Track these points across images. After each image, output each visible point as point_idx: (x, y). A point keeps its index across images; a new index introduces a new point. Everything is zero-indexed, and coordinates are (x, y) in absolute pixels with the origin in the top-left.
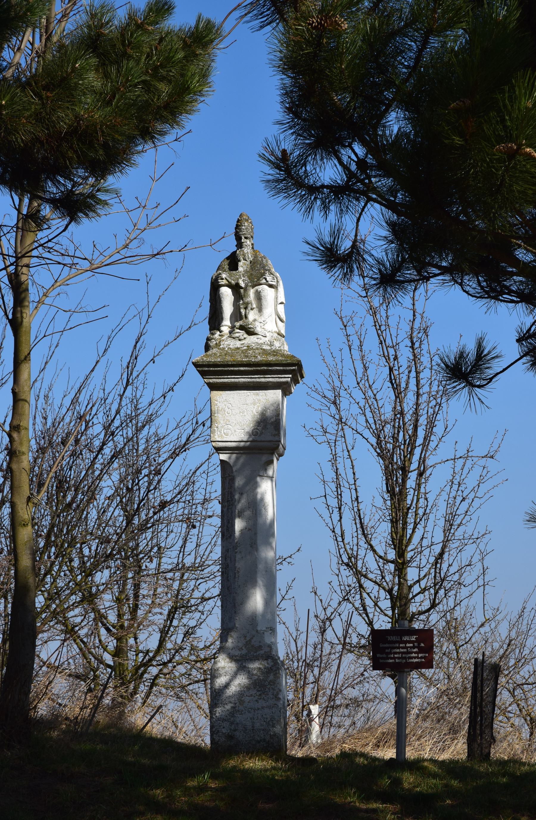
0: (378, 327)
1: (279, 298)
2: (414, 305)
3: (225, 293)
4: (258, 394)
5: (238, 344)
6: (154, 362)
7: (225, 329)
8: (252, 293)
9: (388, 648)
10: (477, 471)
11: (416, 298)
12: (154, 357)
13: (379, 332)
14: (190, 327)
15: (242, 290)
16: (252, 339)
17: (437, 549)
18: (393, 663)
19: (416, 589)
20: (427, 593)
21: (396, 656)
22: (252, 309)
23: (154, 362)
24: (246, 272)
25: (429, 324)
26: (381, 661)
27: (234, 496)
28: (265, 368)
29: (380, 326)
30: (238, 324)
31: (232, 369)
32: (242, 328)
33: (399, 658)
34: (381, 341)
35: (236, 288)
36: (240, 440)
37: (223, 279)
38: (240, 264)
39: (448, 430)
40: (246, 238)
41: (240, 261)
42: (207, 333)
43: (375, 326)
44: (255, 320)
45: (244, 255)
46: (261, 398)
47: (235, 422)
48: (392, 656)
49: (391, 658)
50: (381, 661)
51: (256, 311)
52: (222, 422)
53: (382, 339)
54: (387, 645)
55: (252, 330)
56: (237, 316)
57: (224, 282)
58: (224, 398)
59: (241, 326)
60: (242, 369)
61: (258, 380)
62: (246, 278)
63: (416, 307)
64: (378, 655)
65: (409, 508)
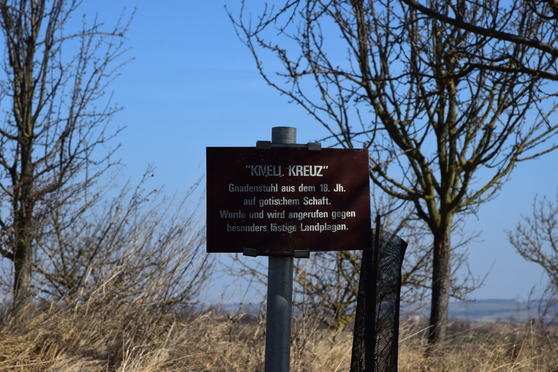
9: (249, 195)
10: (104, 47)
17: (63, 126)
18: (261, 233)
19: (41, 168)
20: (51, 172)
21: (270, 215)
26: (230, 228)
33: (279, 222)
39: (76, 4)
48: (261, 215)
49: (259, 222)
50: (230, 228)
54: (248, 188)
64: (224, 214)
65: (36, 81)
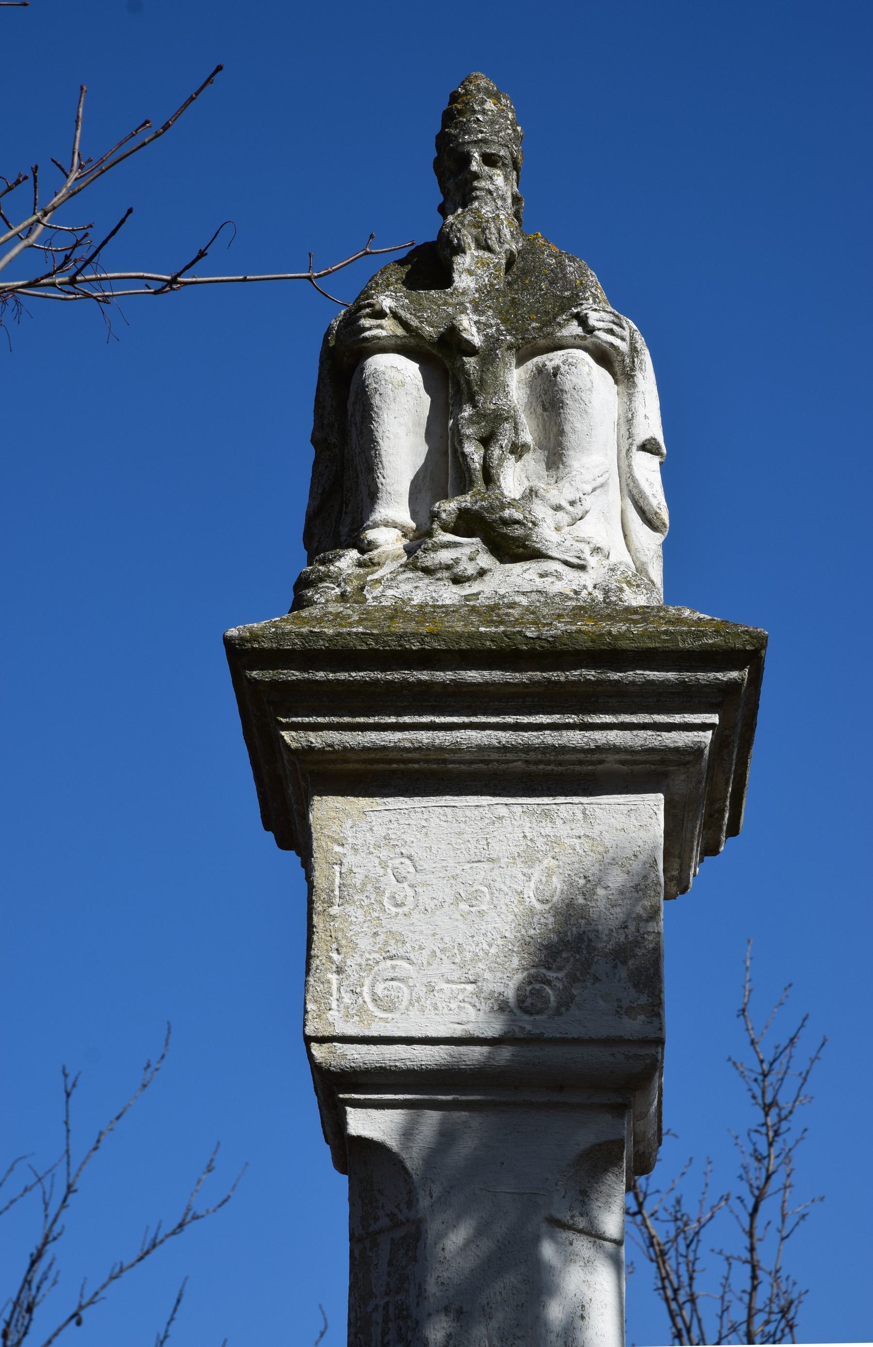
0: (670, 1293)
1: (639, 419)
2: (752, 1249)
3: (391, 374)
4: (546, 814)
5: (449, 594)
6: (79, 1323)
7: (387, 540)
8: (515, 383)
11: (758, 1234)
12: (81, 1307)
13: (674, 1305)
14: (181, 1226)
15: (471, 362)
16: (510, 582)
22: (518, 450)
23: (79, 1323)
24: (487, 292)
25: (794, 1295)
27: (418, 1326)
28: (591, 674)
29: (676, 1291)
30: (449, 507)
31: (424, 676)
32: (467, 524)
34: (679, 1331)
35: (443, 360)
36: (457, 1031)
37: (380, 314)
38: (463, 261)
40: (490, 160)
41: (460, 250)
42: (298, 563)
43: (664, 1288)
44: (532, 493)
45: (480, 225)
46: (562, 830)
47: (431, 945)
51: (533, 461)
52: (364, 943)
53: (680, 1325)
55: (519, 531)
56: (446, 470)
57: (388, 328)
58: (380, 831)
59: (463, 513)
60: (473, 676)
61: (550, 738)
62: (490, 317)
63: (758, 1255)
